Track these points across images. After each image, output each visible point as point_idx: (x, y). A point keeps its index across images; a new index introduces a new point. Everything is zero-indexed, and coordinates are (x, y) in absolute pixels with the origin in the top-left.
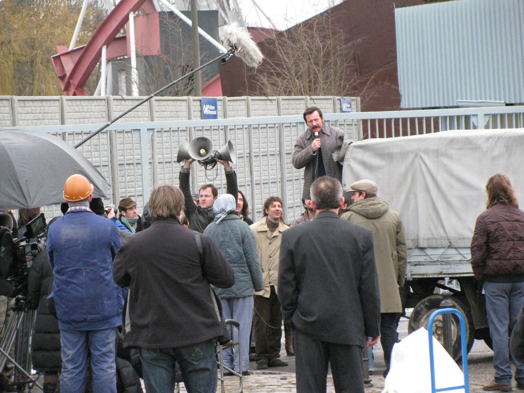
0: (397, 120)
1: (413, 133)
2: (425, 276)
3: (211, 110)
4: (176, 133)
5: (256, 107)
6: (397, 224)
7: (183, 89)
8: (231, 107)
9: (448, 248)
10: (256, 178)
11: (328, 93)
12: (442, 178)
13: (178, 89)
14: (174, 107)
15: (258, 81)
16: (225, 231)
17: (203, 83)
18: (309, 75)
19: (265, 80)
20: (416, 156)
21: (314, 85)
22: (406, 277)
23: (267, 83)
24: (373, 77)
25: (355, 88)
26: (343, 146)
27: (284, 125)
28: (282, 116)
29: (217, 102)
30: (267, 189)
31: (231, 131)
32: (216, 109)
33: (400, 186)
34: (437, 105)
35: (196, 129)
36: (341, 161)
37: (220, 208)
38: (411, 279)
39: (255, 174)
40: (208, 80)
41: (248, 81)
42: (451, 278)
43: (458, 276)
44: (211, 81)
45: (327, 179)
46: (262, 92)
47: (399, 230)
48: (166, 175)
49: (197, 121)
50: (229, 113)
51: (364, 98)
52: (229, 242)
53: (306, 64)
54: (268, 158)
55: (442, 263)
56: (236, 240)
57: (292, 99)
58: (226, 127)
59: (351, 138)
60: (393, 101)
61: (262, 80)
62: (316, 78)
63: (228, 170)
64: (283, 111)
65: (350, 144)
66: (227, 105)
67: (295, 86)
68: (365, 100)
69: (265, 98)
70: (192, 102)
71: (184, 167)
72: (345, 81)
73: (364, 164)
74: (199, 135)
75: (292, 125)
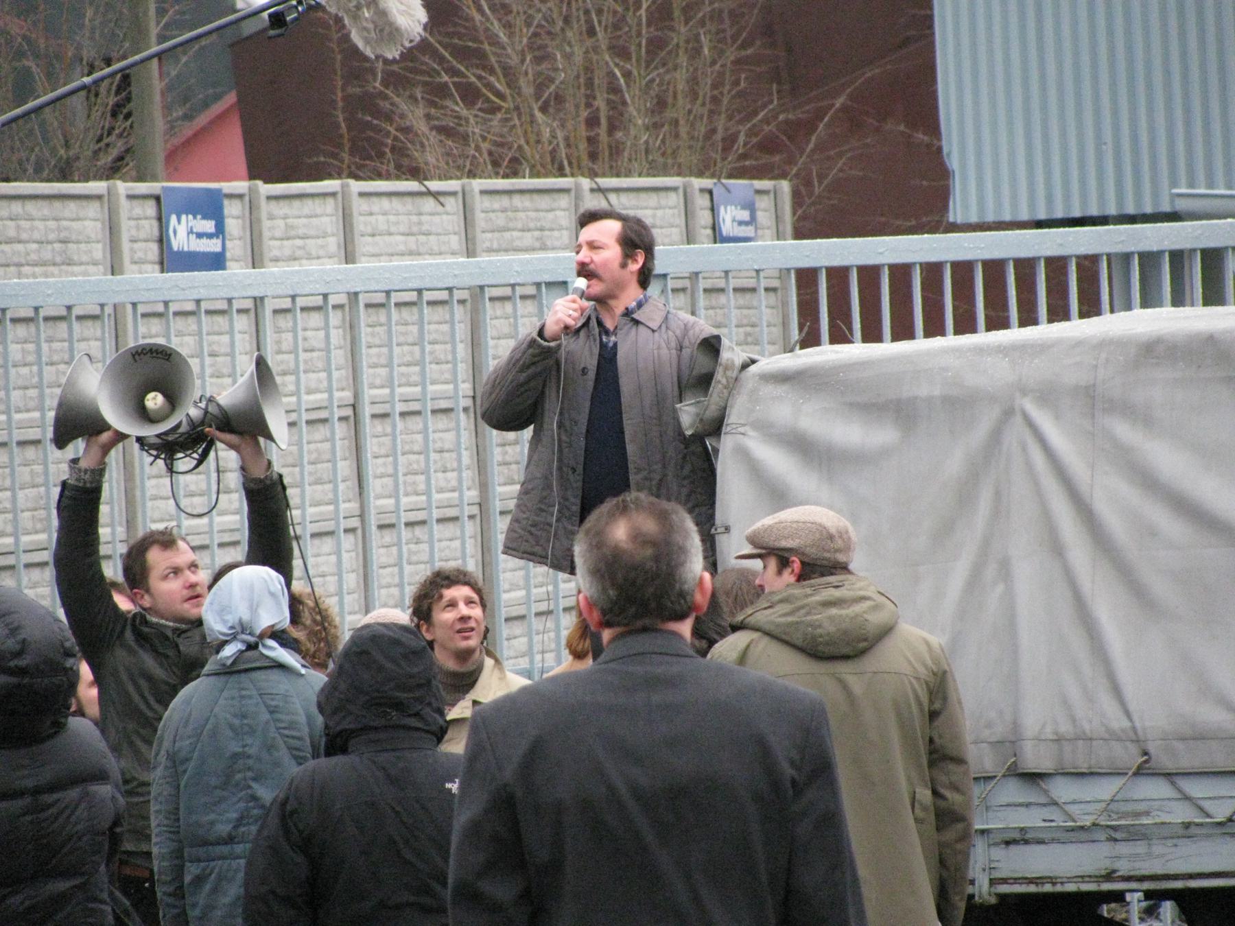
0: (933, 271)
1: (997, 322)
2: (1048, 888)
3: (200, 236)
4: (63, 326)
5: (380, 222)
6: (931, 679)
7: (89, 153)
8: (281, 223)
9: (1136, 774)
10: (379, 503)
11: (665, 166)
12: (1112, 495)
13: (71, 153)
14: (52, 224)
15: (389, 118)
16: (244, 716)
17: (171, 128)
18: (590, 98)
19: (416, 116)
20: (1008, 413)
21: (612, 129)
22: (970, 889)
23: (422, 127)
24: (839, 102)
25: (768, 146)
26: (719, 376)
27: (489, 292)
28: (483, 259)
29: (226, 202)
30: (425, 547)
31: (280, 318)
32: (220, 231)
33: (945, 531)
34: (1094, 211)
35: (141, 309)
36: (709, 435)
37: (232, 619)
38: (993, 901)
39: (375, 486)
40: (188, 117)
41: (350, 121)
42: (1149, 895)
43: (1179, 885)
44: (202, 119)
45: (638, 504)
46: (405, 162)
47: (937, 706)
48: (21, 495)
49: (144, 279)
50: (272, 247)
51: (808, 183)
52: (259, 759)
53: (578, 52)
54: (394, 426)
55: (1114, 834)
56: (290, 748)
57: (522, 192)
58: (259, 301)
59: (756, 343)
60: (920, 196)
61: (402, 116)
62: (617, 107)
63: (258, 472)
64: (484, 239)
65: (745, 366)
66: (264, 215)
67: (533, 138)
68: (811, 194)
69: (412, 185)
70: (123, 202)
71: (83, 464)
72: (730, 118)
73: (802, 446)
74: (150, 334)
75: (519, 291)
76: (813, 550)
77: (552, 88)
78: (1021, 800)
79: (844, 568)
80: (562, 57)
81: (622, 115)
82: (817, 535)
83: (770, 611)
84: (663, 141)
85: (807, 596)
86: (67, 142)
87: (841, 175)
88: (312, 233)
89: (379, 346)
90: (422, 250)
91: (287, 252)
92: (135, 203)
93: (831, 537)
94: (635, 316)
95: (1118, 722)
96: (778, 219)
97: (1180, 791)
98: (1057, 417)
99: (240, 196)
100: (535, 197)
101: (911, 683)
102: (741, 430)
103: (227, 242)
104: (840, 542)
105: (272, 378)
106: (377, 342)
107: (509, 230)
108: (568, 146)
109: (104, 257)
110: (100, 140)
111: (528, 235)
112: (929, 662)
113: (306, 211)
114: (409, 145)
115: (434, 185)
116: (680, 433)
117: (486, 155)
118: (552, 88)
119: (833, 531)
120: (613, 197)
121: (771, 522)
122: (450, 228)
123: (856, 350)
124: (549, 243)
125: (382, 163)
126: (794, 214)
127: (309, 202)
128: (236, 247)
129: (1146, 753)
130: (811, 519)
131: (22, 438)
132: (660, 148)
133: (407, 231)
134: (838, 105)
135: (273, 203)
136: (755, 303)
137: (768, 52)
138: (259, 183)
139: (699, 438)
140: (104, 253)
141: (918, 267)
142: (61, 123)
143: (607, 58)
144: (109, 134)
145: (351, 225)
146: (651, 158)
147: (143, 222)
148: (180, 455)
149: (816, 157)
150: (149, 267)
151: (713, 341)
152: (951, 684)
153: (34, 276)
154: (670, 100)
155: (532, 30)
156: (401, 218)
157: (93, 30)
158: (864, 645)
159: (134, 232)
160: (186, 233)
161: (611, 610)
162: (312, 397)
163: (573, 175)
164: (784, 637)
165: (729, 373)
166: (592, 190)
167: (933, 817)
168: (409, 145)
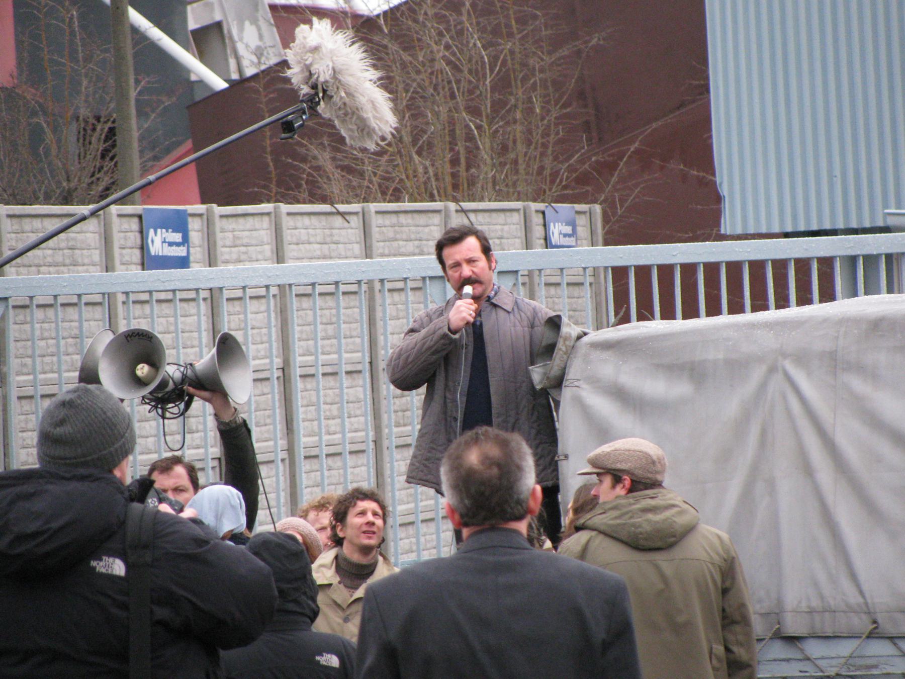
1: (760, 305)
3: (171, 244)
5: (303, 234)
8: (230, 235)
9: (868, 637)
12: (849, 433)
15: (304, 160)
18: (453, 143)
21: (468, 168)
23: (329, 167)
25: (583, 179)
26: (560, 345)
29: (190, 219)
32: (185, 240)
34: (827, 226)
41: (276, 161)
47: (728, 584)
49: (129, 275)
50: (223, 252)
51: (613, 206)
53: (443, 110)
60: (700, 215)
61: (315, 158)
62: (473, 154)
64: (378, 246)
65: (579, 338)
66: (218, 230)
68: (614, 214)
69: (326, 208)
72: (556, 158)
73: (621, 395)
76: (640, 472)
77: (425, 137)
78: (783, 656)
79: (656, 484)
80: (433, 115)
81: (476, 157)
82: (644, 460)
83: (604, 516)
84: (506, 175)
85: (630, 504)
86: (68, 177)
87: (637, 200)
88: (254, 242)
89: (25, 340)
90: (333, 254)
91: (234, 256)
92: (124, 220)
93: (654, 462)
94: (494, 301)
95: (854, 598)
96: (592, 232)
97: (899, 649)
98: (809, 374)
99: (200, 215)
100: (416, 216)
101: (708, 568)
102: (576, 384)
103: (191, 249)
104: (659, 465)
105: (240, 348)
106: (24, 337)
107: (396, 240)
108: (437, 179)
109: (101, 261)
110: (92, 176)
111: (411, 243)
112: (721, 552)
113: (248, 226)
114: (320, 179)
115: (342, 207)
116: (533, 387)
117: (376, 186)
118: (425, 137)
119: (655, 458)
120: (472, 216)
121: (609, 450)
122: (354, 239)
123: (657, 326)
124: (425, 250)
125: (299, 192)
126: (604, 227)
127: (250, 219)
128: (197, 253)
129: (875, 622)
130: (637, 448)
131: (44, 393)
132: (504, 180)
133: (322, 241)
134: (632, 149)
135: (224, 220)
136: (582, 294)
137: (583, 110)
138: (214, 206)
139: (545, 392)
140: (101, 257)
141: (770, 262)
142: (64, 165)
143: (464, 114)
144: (99, 171)
145: (282, 236)
146: (497, 188)
147: (129, 234)
148: (170, 405)
149: (618, 187)
150: (133, 267)
151: (557, 319)
152: (738, 570)
153: (50, 273)
154: (511, 144)
155: (409, 94)
156: (318, 231)
157: (87, 96)
158: (672, 539)
159: (122, 242)
160: (160, 242)
161: (467, 515)
162: (257, 362)
163: (441, 201)
164: (615, 535)
165: (567, 343)
166: (457, 211)
167: (725, 666)
168: (320, 179)
